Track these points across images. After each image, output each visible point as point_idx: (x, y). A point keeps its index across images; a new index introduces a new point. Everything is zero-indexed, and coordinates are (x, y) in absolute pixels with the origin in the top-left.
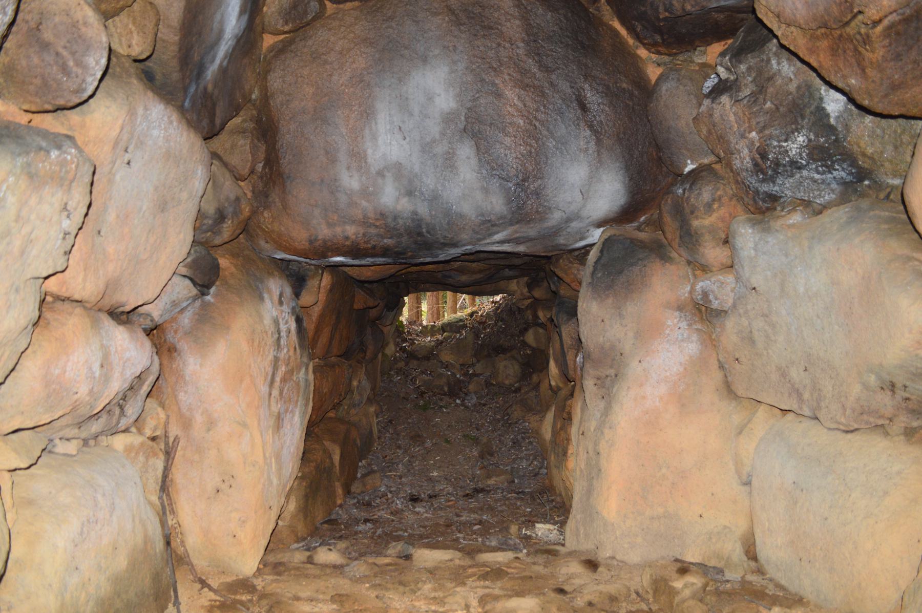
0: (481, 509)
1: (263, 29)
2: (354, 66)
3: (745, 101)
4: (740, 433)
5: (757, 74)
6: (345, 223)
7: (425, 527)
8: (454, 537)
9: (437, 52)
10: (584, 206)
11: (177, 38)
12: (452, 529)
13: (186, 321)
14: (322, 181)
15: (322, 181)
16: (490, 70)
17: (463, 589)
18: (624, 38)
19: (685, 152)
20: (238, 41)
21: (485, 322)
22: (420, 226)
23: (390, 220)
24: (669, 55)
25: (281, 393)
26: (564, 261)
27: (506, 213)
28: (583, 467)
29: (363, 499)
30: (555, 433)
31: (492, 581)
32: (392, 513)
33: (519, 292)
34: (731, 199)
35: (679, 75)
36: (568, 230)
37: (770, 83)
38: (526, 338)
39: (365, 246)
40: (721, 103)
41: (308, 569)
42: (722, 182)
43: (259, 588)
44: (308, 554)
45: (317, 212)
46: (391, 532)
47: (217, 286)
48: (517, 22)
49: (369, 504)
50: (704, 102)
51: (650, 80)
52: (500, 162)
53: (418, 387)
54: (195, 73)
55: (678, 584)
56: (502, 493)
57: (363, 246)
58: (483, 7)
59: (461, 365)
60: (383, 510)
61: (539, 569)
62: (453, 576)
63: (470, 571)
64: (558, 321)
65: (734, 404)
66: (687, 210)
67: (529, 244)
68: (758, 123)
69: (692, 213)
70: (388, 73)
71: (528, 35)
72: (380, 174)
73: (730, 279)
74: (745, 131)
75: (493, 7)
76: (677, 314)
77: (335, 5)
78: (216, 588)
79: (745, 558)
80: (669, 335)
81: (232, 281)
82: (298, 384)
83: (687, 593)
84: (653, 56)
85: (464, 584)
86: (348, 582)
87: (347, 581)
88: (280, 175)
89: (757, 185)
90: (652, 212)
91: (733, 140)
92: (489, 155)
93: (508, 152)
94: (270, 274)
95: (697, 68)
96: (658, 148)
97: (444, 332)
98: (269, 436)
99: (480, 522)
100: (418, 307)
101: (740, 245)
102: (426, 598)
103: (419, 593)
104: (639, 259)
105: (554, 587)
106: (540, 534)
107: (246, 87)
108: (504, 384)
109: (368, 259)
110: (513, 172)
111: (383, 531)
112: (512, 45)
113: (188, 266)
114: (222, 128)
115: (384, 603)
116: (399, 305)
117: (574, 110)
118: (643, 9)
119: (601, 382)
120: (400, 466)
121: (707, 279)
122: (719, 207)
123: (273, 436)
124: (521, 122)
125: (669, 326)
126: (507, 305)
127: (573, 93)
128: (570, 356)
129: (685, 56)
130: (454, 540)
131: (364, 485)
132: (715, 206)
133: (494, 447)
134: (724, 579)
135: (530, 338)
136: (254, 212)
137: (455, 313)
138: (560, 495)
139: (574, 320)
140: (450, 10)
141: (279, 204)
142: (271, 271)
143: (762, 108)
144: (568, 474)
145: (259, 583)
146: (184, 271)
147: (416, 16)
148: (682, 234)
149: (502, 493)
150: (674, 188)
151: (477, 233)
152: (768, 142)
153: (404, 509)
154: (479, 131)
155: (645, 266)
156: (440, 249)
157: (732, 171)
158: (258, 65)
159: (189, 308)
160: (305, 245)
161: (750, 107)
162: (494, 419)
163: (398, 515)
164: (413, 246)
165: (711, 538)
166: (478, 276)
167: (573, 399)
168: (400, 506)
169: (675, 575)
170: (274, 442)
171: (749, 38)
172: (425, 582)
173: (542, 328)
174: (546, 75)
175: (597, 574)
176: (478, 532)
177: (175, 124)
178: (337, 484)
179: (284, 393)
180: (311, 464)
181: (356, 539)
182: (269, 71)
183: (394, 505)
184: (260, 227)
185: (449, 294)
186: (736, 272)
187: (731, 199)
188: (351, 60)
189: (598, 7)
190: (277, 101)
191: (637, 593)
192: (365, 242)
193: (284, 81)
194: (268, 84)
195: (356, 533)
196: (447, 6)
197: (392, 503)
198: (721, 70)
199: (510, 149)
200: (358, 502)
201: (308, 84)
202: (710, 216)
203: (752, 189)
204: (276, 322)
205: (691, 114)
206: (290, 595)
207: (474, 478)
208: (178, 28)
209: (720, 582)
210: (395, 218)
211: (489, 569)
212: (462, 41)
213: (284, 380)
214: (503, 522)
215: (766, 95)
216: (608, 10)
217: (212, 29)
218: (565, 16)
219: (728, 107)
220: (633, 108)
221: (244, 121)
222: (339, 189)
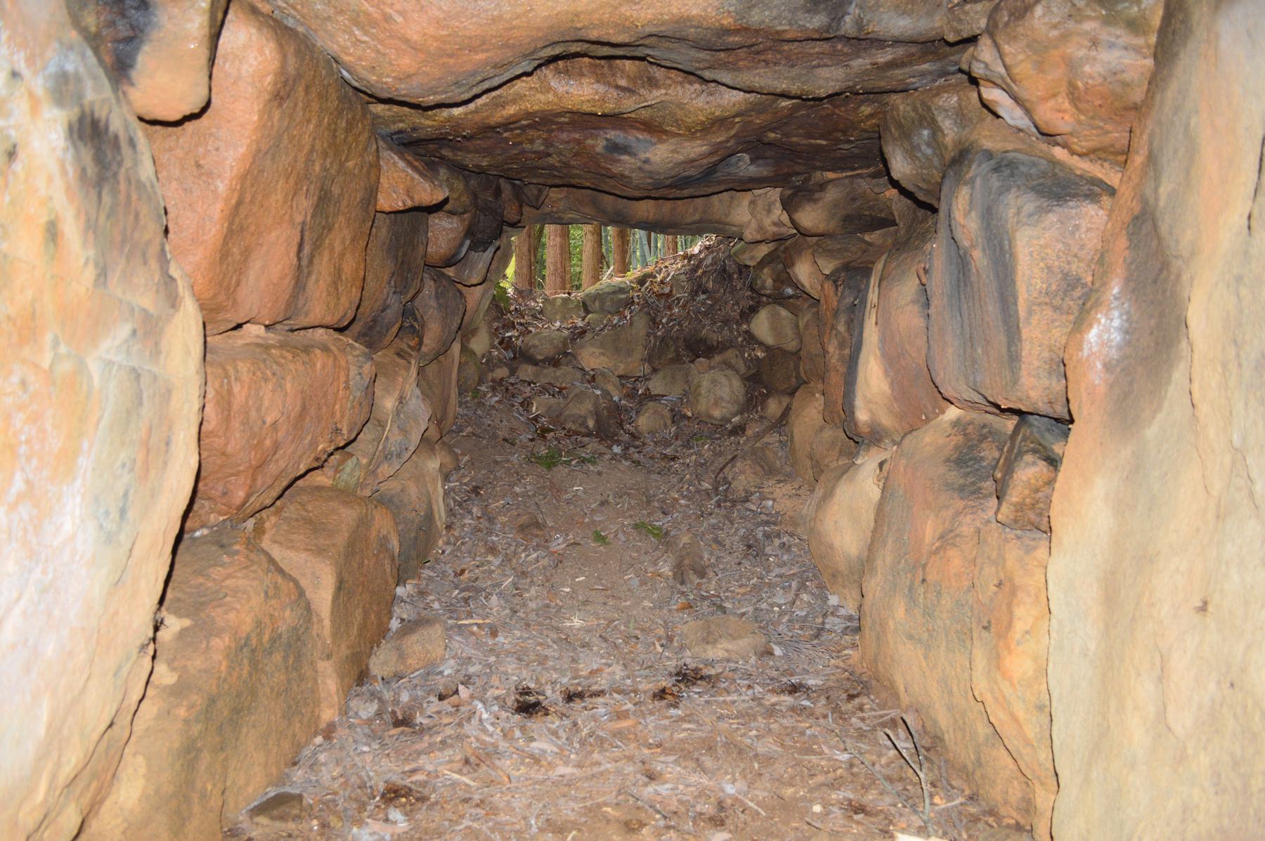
21: (669, 295)
29: (396, 702)
33: (754, 225)
38: (753, 325)
53: (536, 419)
59: (620, 377)
97: (587, 312)
108: (711, 417)
131: (402, 657)
133: (706, 556)
162: (698, 491)
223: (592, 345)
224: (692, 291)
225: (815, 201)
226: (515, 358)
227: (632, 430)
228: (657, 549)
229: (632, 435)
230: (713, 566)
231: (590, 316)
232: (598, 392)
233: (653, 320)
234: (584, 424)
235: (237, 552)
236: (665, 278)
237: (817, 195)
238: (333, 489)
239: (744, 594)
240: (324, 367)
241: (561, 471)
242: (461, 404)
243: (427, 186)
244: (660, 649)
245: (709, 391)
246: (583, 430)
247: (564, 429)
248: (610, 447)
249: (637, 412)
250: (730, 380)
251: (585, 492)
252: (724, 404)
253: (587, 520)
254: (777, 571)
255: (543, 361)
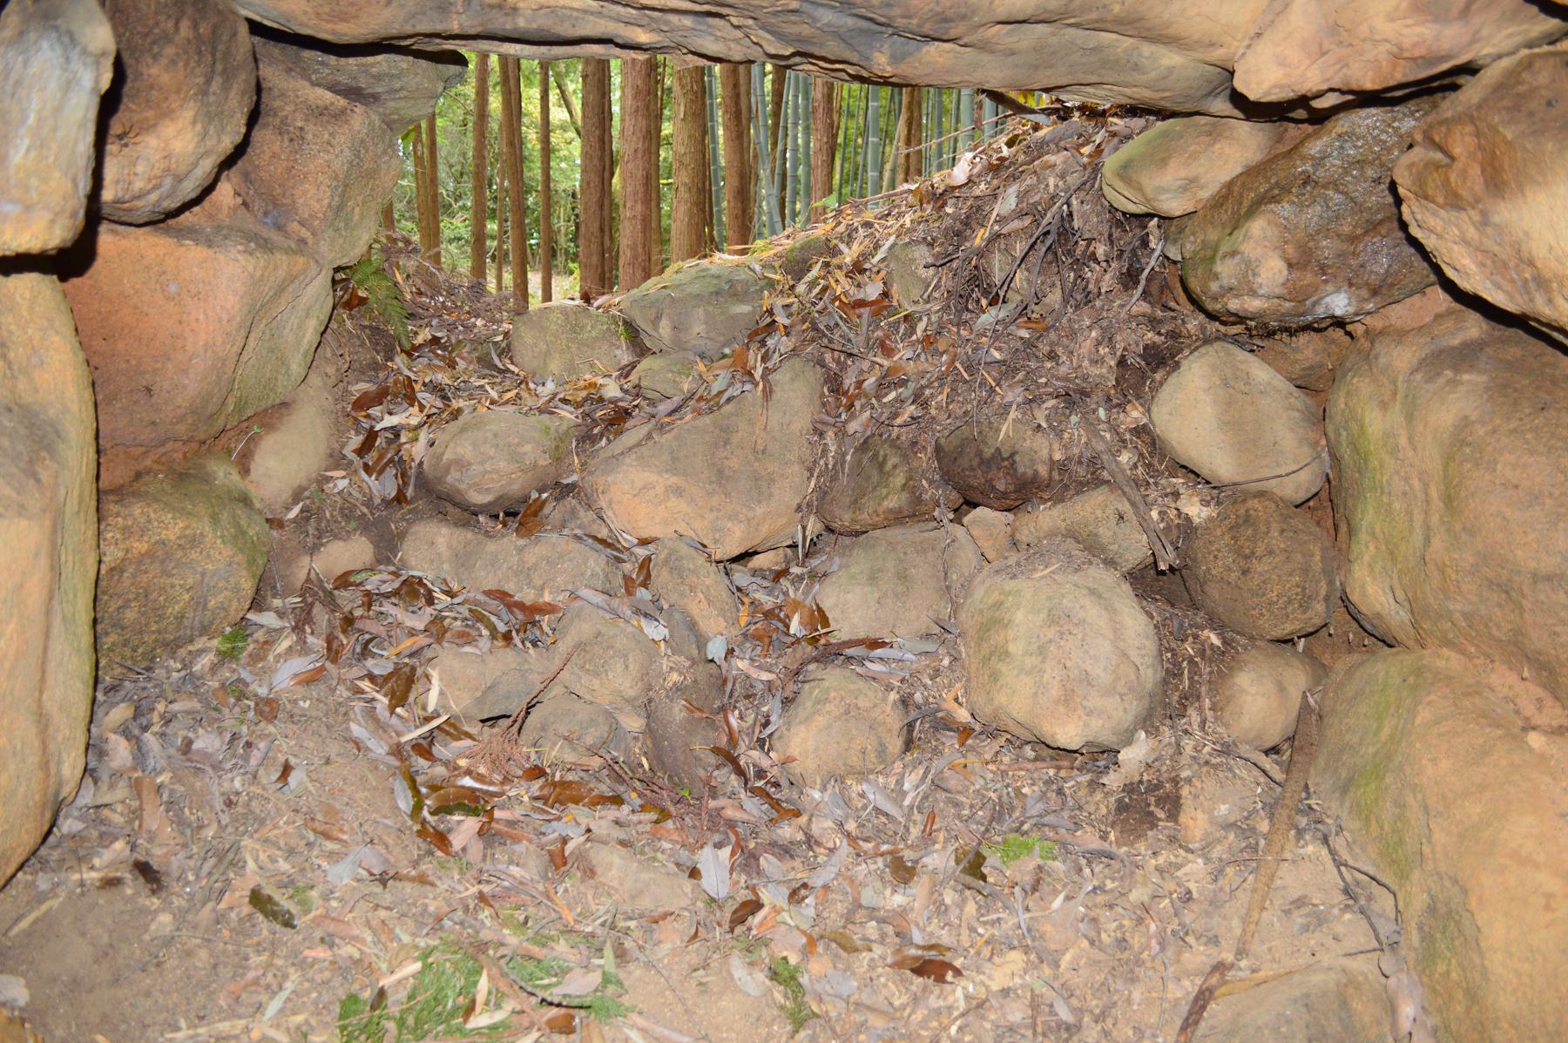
226: (400, 498)
232: (656, 631)
233: (834, 383)
236: (865, 256)
245: (1042, 651)
249: (787, 702)
250: (1111, 610)
252: (1095, 701)
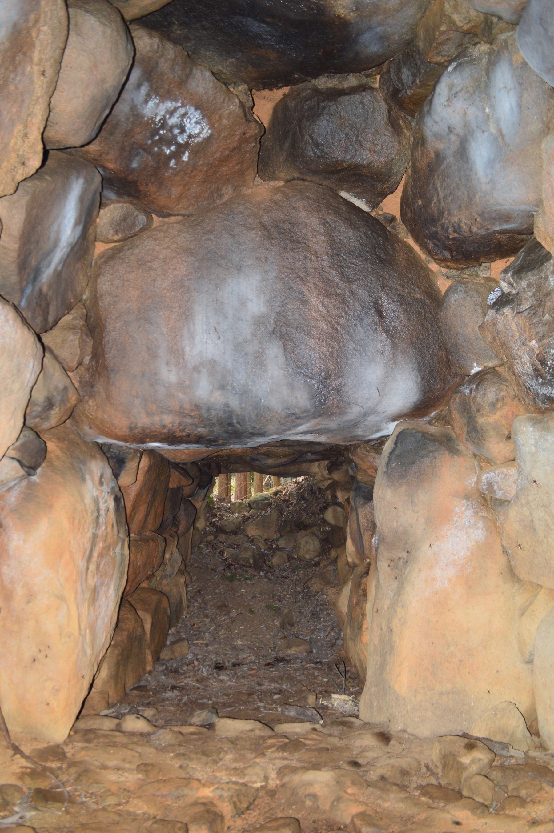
0: (281, 678)
1: (96, 238)
2: (176, 273)
3: (526, 313)
4: (523, 614)
5: (536, 290)
6: (162, 412)
7: (228, 695)
8: (256, 706)
9: (250, 262)
10: (380, 402)
11: (16, 246)
12: (253, 698)
13: (13, 499)
14: (143, 374)
15: (143, 374)
16: (298, 279)
17: (263, 760)
18: (417, 253)
19: (472, 356)
20: (73, 248)
21: (288, 501)
22: (231, 417)
23: (203, 411)
24: (457, 270)
25: (98, 568)
26: (361, 449)
27: (309, 407)
28: (376, 642)
29: (171, 666)
30: (351, 608)
31: (290, 752)
32: (198, 680)
33: (320, 474)
34: (513, 399)
35: (466, 287)
36: (366, 423)
37: (548, 298)
38: (325, 516)
39: (181, 434)
40: (503, 314)
41: (116, 736)
42: (505, 383)
43: (69, 755)
44: (117, 721)
45: (137, 402)
46: (196, 699)
47: (43, 467)
48: (322, 238)
49: (176, 671)
50: (489, 313)
51: (440, 292)
52: (304, 361)
53: (226, 560)
54: (32, 276)
55: (466, 760)
56: (301, 662)
57: (178, 434)
58: (292, 224)
59: (265, 540)
60: (189, 677)
61: (335, 741)
62: (253, 747)
63: (270, 741)
64: (355, 504)
65: (517, 586)
66: (474, 409)
67: (330, 435)
68: (537, 333)
69: (478, 411)
70: (206, 280)
71: (332, 249)
72: (196, 369)
73: (513, 471)
74: (525, 339)
75: (301, 224)
76: (464, 502)
77: (160, 219)
78: (27, 754)
79: (528, 734)
80: (457, 521)
81: (56, 463)
82: (114, 559)
83: (474, 768)
84: (443, 270)
85: (263, 755)
86: (154, 751)
87: (153, 750)
88: (106, 368)
89: (536, 388)
90: (441, 408)
91: (515, 346)
92: (295, 355)
93: (312, 352)
94: (93, 457)
95: (482, 282)
96: (447, 352)
97: (251, 508)
98: (84, 610)
99: (280, 692)
100: (227, 484)
101: (522, 442)
102: (227, 769)
103: (221, 763)
104: (429, 452)
105: (349, 760)
106: (336, 704)
107: (78, 289)
108: (305, 558)
109: (183, 445)
110: (316, 371)
111: (189, 699)
112: (317, 257)
113: (18, 449)
114: (56, 323)
115: (188, 773)
116: (210, 484)
117: (372, 316)
118: (434, 229)
119: (394, 563)
120: (207, 634)
121: (491, 471)
122: (503, 406)
123: (89, 610)
124: (325, 326)
125: (457, 513)
126: (308, 486)
127: (372, 301)
128: (366, 537)
129: (472, 270)
130: (255, 709)
131: (173, 652)
132: (499, 405)
133: (295, 618)
134: (509, 755)
135: (329, 515)
136: (80, 401)
137: (262, 491)
138: (355, 666)
139: (370, 504)
140: (263, 226)
141: (103, 395)
142: (93, 454)
143: (541, 320)
144: (363, 647)
145: (69, 750)
146: (12, 453)
147: (233, 231)
148: (469, 430)
149: (301, 662)
150: (462, 388)
151: (283, 424)
152: (547, 350)
153: (210, 677)
154: (287, 334)
155: (435, 458)
156: (249, 438)
157: (514, 374)
158: (89, 269)
159: (16, 487)
160: (125, 432)
161: (530, 319)
162: (295, 592)
163: (203, 683)
164: (224, 435)
165: (496, 714)
166: (283, 460)
167: (369, 577)
168: (205, 674)
169: (463, 751)
170: (89, 614)
171: (529, 258)
172: (226, 752)
173: (340, 506)
174: (347, 285)
175: (390, 746)
176: (278, 701)
177: (11, 322)
178: (148, 651)
179: (101, 567)
180: (124, 633)
181: (163, 706)
182: (99, 275)
183: (200, 672)
184: (84, 414)
185: (256, 474)
186: (519, 465)
187: (513, 399)
188: (173, 267)
189: (394, 226)
190: (105, 302)
191: (427, 767)
192: (180, 431)
193: (112, 285)
194: (98, 286)
195: (163, 700)
196: (260, 223)
197: (198, 671)
198: (504, 285)
199: (314, 350)
200: (167, 669)
201: (133, 287)
202: (495, 414)
203: (533, 391)
204: (96, 501)
205: (477, 322)
206: (97, 764)
207: (275, 648)
208: (18, 237)
209: (505, 757)
210: (209, 410)
211: (287, 740)
212: (273, 253)
213: (101, 555)
214: (302, 691)
215: (544, 309)
216: (403, 229)
217: (49, 238)
218: (365, 233)
219: (510, 317)
220: (425, 316)
221: (75, 318)
222: (158, 382)
223: (252, 525)
224: (298, 499)
225: (339, 470)
226: (217, 531)
227: (270, 564)
228: (274, 616)
229: (270, 567)
230: (297, 622)
231: (251, 511)
232: (254, 547)
234: (248, 561)
235: (127, 607)
236: (286, 492)
237: (340, 467)
238: (148, 588)
239: (308, 633)
240: (153, 546)
241: (236, 583)
242: (192, 553)
243: (185, 480)
244: (270, 651)
246: (248, 565)
247: (239, 564)
248: (259, 573)
251: (246, 592)
252: (311, 552)
253: (246, 604)
254: (323, 624)
255: (230, 532)
